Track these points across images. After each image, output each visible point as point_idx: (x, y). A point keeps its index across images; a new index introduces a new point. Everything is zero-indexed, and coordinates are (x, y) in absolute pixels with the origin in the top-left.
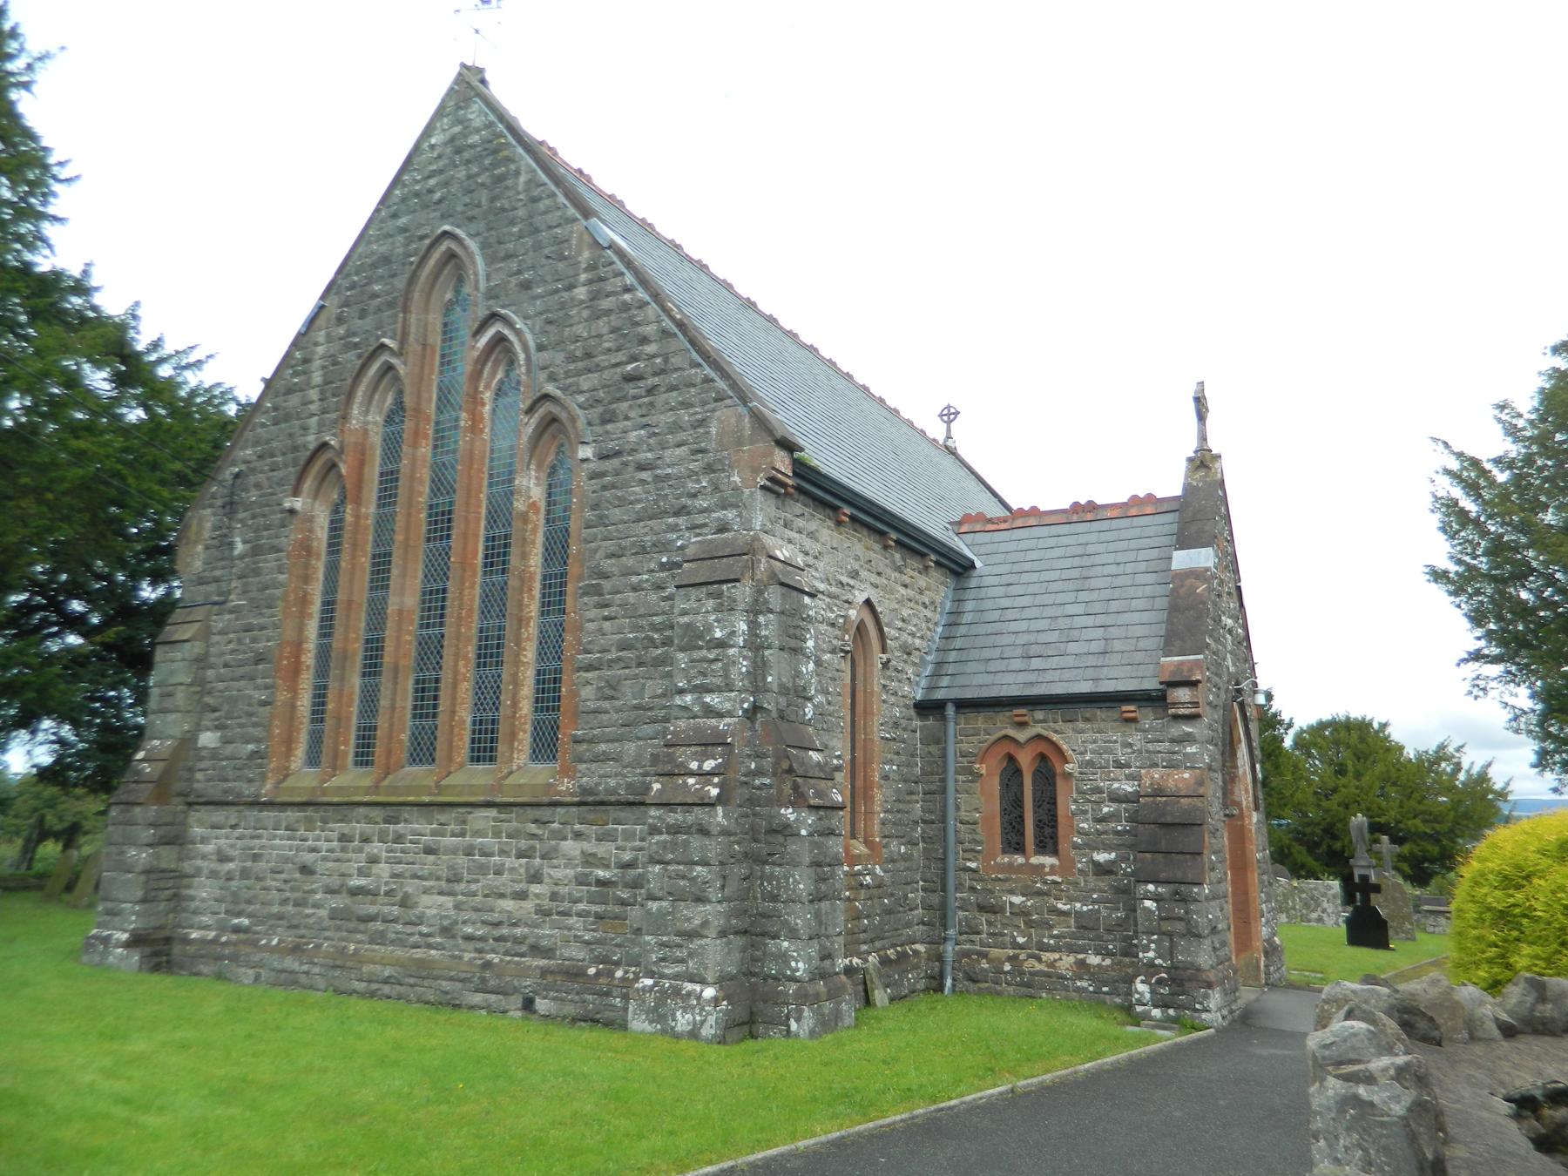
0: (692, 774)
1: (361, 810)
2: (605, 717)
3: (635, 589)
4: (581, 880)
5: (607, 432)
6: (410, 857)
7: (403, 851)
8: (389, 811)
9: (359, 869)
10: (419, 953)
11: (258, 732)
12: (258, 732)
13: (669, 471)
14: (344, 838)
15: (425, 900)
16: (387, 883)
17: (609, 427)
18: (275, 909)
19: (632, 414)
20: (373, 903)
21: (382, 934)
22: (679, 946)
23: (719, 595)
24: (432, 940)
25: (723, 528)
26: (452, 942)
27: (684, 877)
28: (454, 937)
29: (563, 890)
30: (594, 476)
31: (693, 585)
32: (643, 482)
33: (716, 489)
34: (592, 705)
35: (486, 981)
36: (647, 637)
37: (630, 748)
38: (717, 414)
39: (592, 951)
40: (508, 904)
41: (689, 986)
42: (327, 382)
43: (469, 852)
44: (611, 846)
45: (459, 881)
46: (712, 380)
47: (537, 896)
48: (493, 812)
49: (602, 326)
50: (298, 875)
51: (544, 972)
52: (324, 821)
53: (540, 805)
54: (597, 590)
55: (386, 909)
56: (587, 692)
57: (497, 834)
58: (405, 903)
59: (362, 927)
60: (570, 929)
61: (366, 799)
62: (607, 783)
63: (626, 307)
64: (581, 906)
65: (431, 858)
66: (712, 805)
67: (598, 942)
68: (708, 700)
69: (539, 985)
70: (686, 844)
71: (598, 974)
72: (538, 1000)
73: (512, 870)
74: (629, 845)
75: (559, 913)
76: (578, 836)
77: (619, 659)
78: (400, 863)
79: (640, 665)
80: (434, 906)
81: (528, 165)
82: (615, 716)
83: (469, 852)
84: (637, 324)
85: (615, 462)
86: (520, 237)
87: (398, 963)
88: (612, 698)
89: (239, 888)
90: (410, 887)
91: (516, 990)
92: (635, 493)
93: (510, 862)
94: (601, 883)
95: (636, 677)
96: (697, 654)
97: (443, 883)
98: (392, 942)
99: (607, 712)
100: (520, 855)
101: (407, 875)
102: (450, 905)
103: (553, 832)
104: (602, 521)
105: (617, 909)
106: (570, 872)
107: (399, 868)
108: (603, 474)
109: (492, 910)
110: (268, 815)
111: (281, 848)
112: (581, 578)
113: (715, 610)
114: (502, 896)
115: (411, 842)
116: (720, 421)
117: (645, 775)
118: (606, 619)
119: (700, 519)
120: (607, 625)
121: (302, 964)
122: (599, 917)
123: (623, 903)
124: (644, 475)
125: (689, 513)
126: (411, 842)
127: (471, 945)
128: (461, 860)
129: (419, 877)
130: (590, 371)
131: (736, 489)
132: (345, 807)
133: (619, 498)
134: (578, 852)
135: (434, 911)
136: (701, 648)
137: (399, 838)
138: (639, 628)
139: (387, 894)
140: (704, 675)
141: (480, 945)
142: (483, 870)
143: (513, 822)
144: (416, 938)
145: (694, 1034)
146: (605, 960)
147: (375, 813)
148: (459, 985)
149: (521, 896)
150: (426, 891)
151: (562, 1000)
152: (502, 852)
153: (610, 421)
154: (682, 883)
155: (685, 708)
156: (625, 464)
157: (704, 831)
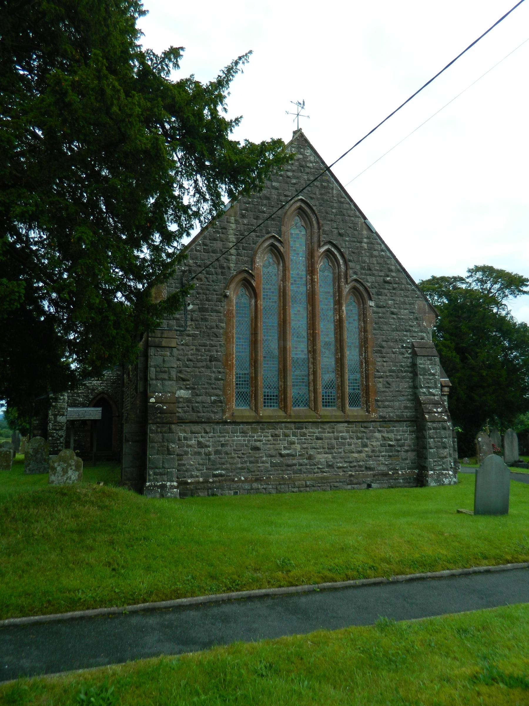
0: (436, 413)
1: (283, 425)
2: (387, 394)
3: (394, 353)
4: (382, 446)
5: (379, 299)
6: (309, 441)
7: (305, 439)
8: (298, 425)
9: (284, 447)
10: (320, 475)
11: (218, 392)
12: (218, 392)
13: (403, 317)
14: (274, 436)
15: (319, 456)
16: (299, 452)
17: (380, 297)
18: (240, 466)
19: (388, 295)
20: (294, 459)
21: (300, 470)
22: (440, 461)
23: (431, 360)
24: (324, 470)
25: (423, 338)
26: (333, 470)
27: (439, 442)
28: (333, 468)
29: (377, 449)
30: (374, 312)
31: (424, 356)
32: (394, 318)
33: (419, 326)
34: (382, 390)
35: (351, 481)
36: (399, 369)
37: (397, 404)
38: (417, 302)
39: (388, 467)
40: (356, 455)
41: (444, 472)
42: (239, 241)
43: (337, 438)
44: (392, 434)
45: (333, 448)
46: (415, 291)
47: (366, 451)
48: (346, 425)
49: (374, 260)
50: (250, 451)
51: (374, 476)
52: (263, 429)
53: (364, 423)
54: (380, 352)
55: (301, 461)
56: (380, 385)
57: (348, 432)
58: (310, 458)
59: (289, 468)
60: (379, 461)
61: (285, 420)
62: (389, 415)
63: (383, 257)
64: (383, 454)
65: (320, 441)
66: (446, 421)
67: (391, 464)
68: (431, 391)
69: (373, 480)
70: (440, 433)
71: (393, 474)
72: (373, 484)
73: (355, 444)
74: (398, 434)
75: (375, 456)
76: (379, 431)
77: (390, 375)
78: (305, 443)
79: (398, 378)
80: (322, 458)
81: (336, 186)
82: (390, 394)
83: (337, 438)
84: (388, 264)
85: (384, 310)
86: (336, 215)
87: (312, 479)
88: (389, 388)
89: (216, 458)
90: (311, 452)
91: (364, 482)
92: (391, 322)
93: (355, 441)
94: (390, 445)
95: (396, 381)
96: (426, 377)
97: (327, 450)
98: (305, 473)
99: (387, 392)
100: (358, 438)
101: (309, 448)
102: (330, 457)
103: (371, 430)
104: (380, 329)
105: (396, 454)
106: (379, 443)
107: (305, 446)
108: (378, 313)
109: (349, 458)
110: (230, 427)
111: (240, 440)
112: (373, 347)
113: (431, 364)
114: (353, 452)
115: (309, 436)
116: (418, 305)
117: (402, 412)
118: (384, 362)
119: (415, 334)
120: (385, 364)
121: (261, 485)
122: (390, 456)
123: (398, 451)
124: (395, 316)
125: (410, 332)
126: (309, 436)
127: (341, 470)
128: (334, 441)
129: (315, 448)
130: (370, 275)
131: (425, 327)
132: (273, 424)
133: (386, 322)
134: (381, 437)
135: (323, 460)
136: (426, 375)
137: (304, 435)
138: (396, 366)
139: (299, 455)
140: (428, 383)
141: (345, 470)
142: (343, 444)
143: (354, 428)
144: (316, 470)
145: (450, 484)
146: (394, 469)
147: (292, 426)
148: (341, 484)
149: (360, 452)
150: (319, 453)
151: (382, 483)
152: (351, 438)
153: (380, 295)
154: (440, 444)
155: (424, 393)
156: (387, 311)
157: (444, 428)
